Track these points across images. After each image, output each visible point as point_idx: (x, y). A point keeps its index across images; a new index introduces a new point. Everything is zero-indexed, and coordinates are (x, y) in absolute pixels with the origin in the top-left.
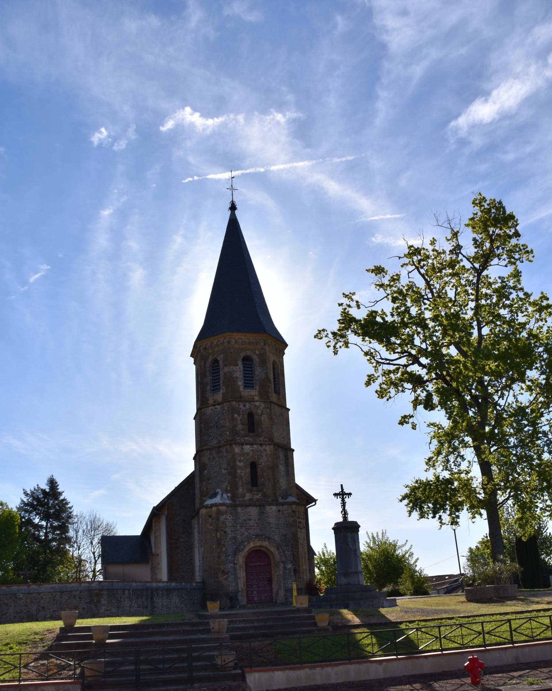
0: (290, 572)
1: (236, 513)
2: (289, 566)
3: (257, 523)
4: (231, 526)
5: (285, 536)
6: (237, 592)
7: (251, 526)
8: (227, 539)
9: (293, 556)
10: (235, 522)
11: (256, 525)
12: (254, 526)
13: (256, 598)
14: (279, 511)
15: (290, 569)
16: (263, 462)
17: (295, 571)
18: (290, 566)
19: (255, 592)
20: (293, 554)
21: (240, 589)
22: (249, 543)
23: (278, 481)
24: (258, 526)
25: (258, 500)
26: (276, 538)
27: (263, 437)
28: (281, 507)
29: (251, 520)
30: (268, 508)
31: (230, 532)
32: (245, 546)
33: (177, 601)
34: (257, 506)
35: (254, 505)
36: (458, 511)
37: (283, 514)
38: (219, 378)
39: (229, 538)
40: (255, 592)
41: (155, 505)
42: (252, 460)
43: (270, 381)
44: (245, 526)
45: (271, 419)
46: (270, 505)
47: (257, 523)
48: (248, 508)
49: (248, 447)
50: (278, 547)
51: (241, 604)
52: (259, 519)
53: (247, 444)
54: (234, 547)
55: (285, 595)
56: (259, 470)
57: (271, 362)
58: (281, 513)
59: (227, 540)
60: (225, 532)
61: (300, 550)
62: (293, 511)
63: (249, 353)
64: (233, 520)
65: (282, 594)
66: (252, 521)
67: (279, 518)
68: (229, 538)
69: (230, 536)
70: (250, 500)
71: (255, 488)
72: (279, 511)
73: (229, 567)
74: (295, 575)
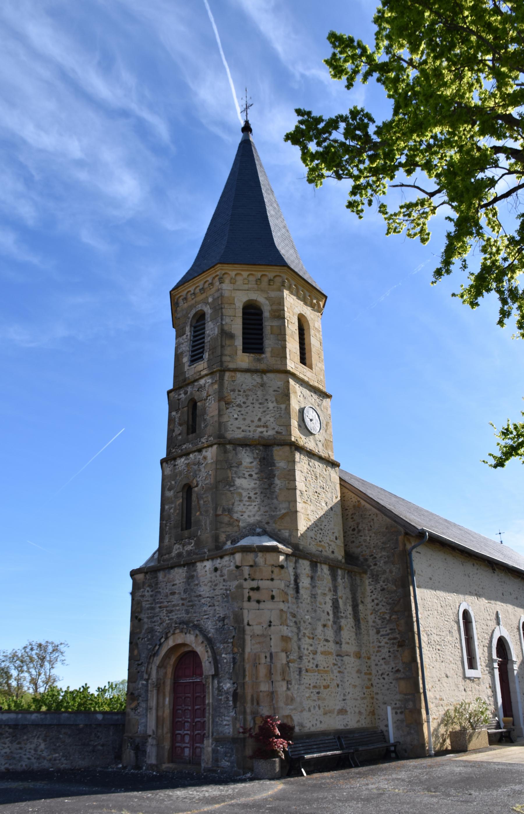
0: (227, 698)
1: (157, 584)
2: (227, 686)
3: (182, 599)
4: (148, 609)
5: (223, 619)
6: (145, 737)
7: (174, 606)
8: (141, 632)
9: (234, 663)
10: (154, 600)
11: (181, 602)
12: (178, 605)
13: (187, 752)
14: (216, 570)
15: (227, 693)
16: (204, 478)
17: (235, 695)
18: (228, 685)
19: (187, 739)
20: (234, 658)
21: (149, 732)
22: (167, 638)
23: (230, 511)
24: (183, 604)
25: (189, 553)
26: (210, 626)
27: (206, 437)
28: (219, 561)
29: (173, 593)
30: (199, 564)
31: (146, 620)
32: (160, 645)
33: (42, 746)
34: (184, 566)
35: (180, 566)
36: (357, 558)
37: (222, 576)
38: (204, 342)
39: (143, 631)
40: (187, 739)
41: (135, 568)
42: (184, 482)
43: (231, 336)
44: (166, 607)
45: (221, 398)
46: (202, 560)
47: (182, 599)
48: (172, 571)
49: (183, 460)
50: (210, 642)
51: (149, 762)
52: (185, 591)
53: (181, 456)
54: (150, 647)
55: (214, 751)
56: (194, 497)
57: (239, 305)
58: (219, 572)
59: (141, 636)
60: (140, 620)
61: (248, 650)
62: (237, 567)
63: (199, 307)
64: (151, 596)
65: (210, 749)
66: (176, 596)
67: (216, 585)
68: (143, 631)
69: (146, 626)
70: (179, 555)
71: (186, 533)
72: (216, 570)
73: (140, 686)
74: (235, 707)
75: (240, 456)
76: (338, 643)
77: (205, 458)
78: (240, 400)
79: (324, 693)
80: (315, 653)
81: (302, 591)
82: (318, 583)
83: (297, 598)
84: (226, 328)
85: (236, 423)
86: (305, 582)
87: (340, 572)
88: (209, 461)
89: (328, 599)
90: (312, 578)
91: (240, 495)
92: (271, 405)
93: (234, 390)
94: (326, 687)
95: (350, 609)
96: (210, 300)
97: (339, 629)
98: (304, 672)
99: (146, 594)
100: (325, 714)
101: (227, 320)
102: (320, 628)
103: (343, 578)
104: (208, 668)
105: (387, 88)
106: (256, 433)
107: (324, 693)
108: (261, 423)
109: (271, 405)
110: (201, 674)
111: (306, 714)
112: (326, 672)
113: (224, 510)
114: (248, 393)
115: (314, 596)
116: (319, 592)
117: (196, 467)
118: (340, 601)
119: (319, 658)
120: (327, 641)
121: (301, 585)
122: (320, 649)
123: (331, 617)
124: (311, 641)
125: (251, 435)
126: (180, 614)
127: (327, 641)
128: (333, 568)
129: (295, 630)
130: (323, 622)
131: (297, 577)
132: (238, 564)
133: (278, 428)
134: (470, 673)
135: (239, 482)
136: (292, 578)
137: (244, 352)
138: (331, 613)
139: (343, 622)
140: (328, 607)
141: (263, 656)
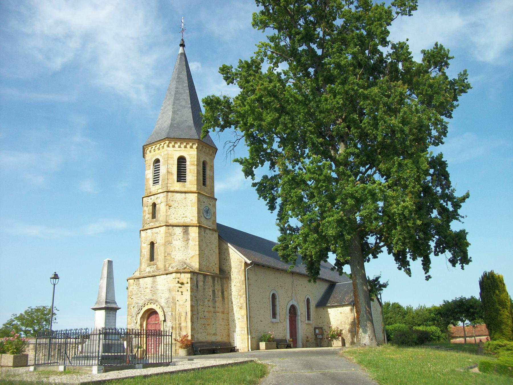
43: (172, 174)
75: (175, 231)
76: (214, 308)
77: (160, 231)
78: (176, 205)
79: (207, 327)
80: (204, 311)
81: (199, 287)
82: (206, 284)
83: (197, 290)
84: (169, 170)
85: (173, 216)
86: (201, 284)
87: (216, 279)
88: (162, 232)
89: (211, 290)
90: (204, 282)
91: (175, 247)
92: (189, 208)
93: (173, 201)
94: (208, 325)
95: (220, 294)
96: (162, 154)
97: (215, 302)
98: (199, 319)
99: (134, 288)
100: (208, 335)
101: (170, 166)
102: (206, 302)
103: (218, 281)
104: (162, 318)
105: (237, 98)
106: (181, 221)
107: (207, 327)
108: (184, 216)
109: (189, 208)
110: (159, 320)
111: (200, 335)
112: (208, 319)
113: (168, 254)
114: (179, 202)
115: (204, 289)
116: (207, 287)
117: (156, 235)
118: (216, 291)
119: (206, 314)
120: (209, 307)
121: (199, 285)
122: (206, 310)
123: (212, 297)
124: (202, 307)
125: (180, 221)
126: (149, 297)
127: (209, 307)
128: (213, 277)
129: (196, 303)
130: (208, 299)
131: (197, 281)
132: (181, 48)
133: (192, 218)
134: (274, 320)
135: (174, 242)
136: (195, 282)
137: (177, 182)
138: (212, 296)
139: (217, 299)
140: (211, 293)
141: (183, 313)
